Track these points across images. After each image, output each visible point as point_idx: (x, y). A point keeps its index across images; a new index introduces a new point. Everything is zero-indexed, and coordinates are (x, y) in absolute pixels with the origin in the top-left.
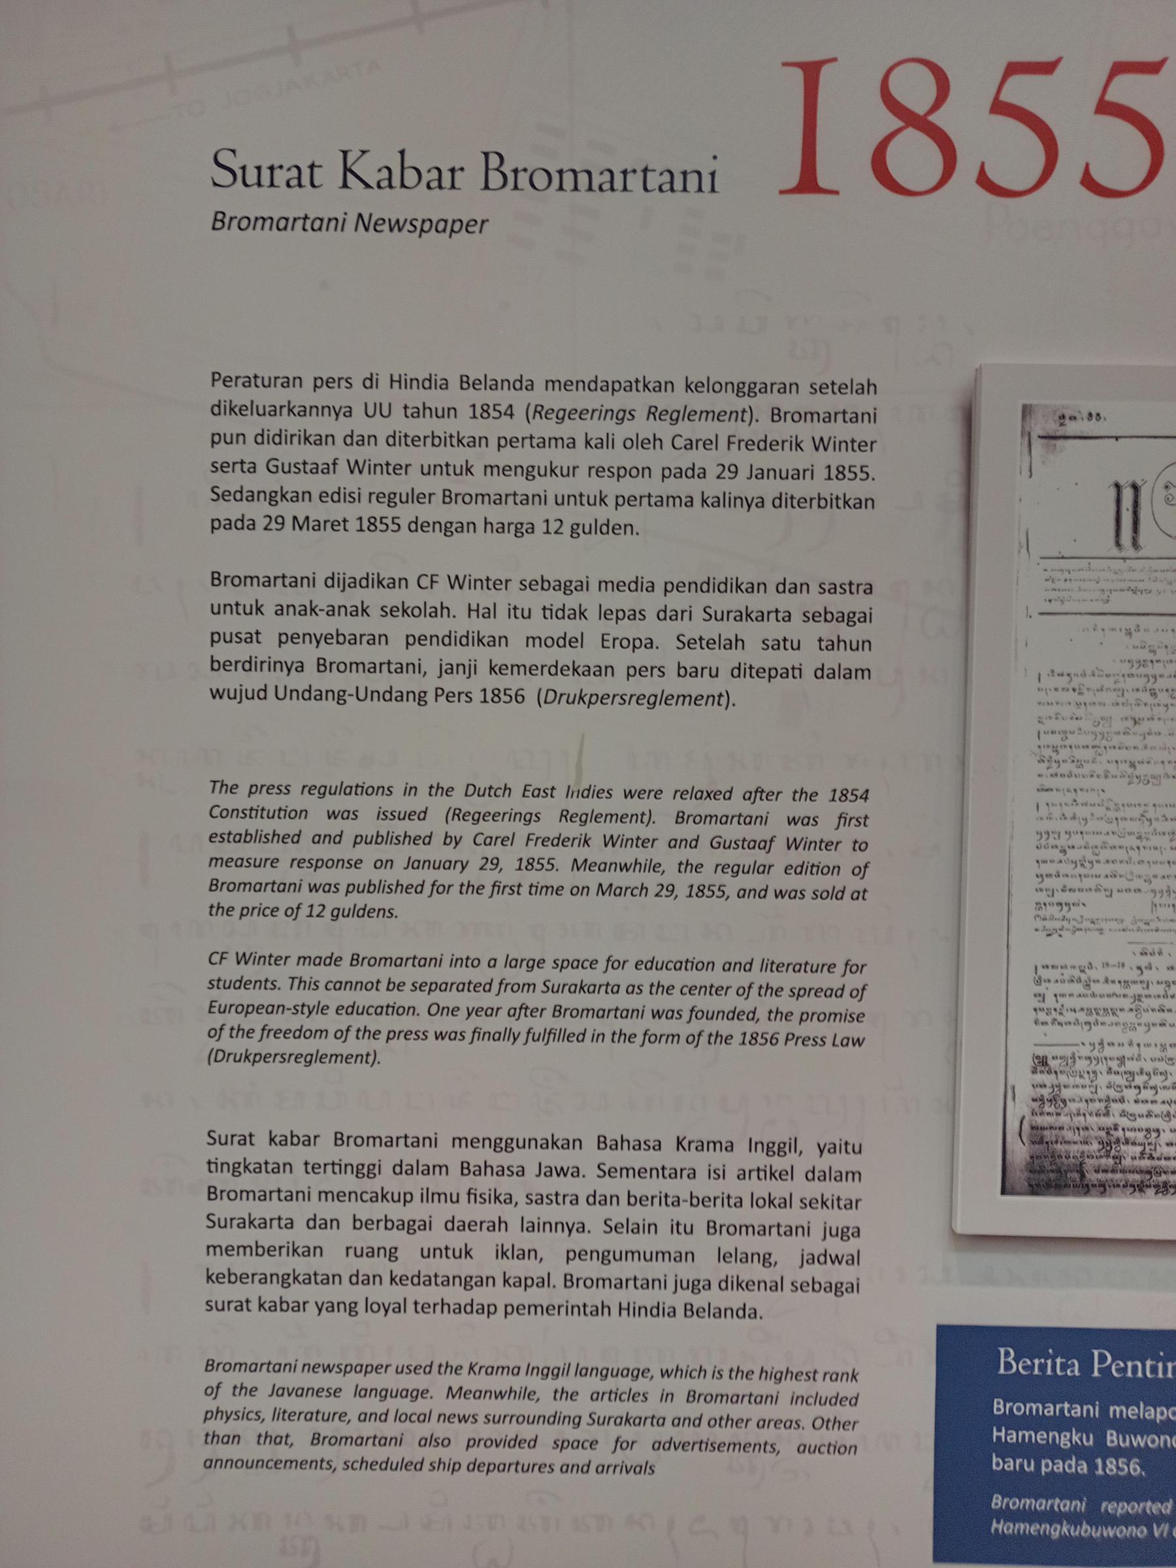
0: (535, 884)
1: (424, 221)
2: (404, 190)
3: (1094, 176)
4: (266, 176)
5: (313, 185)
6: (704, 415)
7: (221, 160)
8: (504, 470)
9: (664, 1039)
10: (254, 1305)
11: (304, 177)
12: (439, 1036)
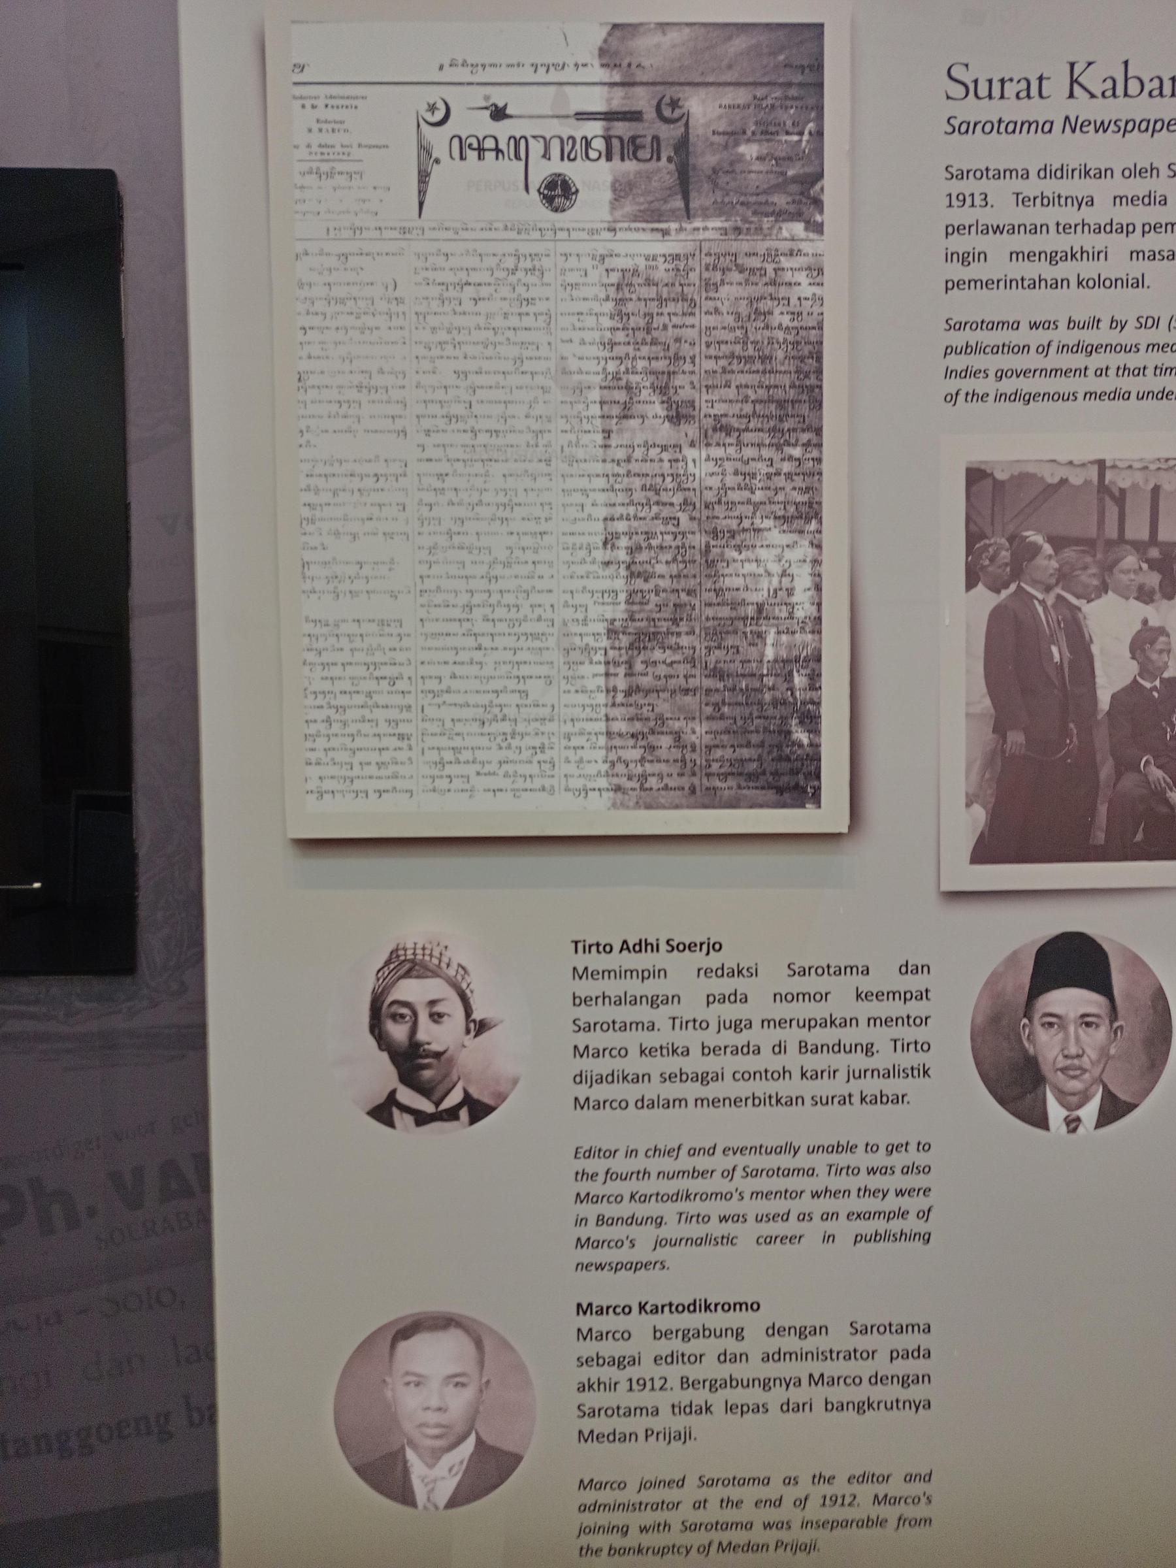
10: (856, 1099)
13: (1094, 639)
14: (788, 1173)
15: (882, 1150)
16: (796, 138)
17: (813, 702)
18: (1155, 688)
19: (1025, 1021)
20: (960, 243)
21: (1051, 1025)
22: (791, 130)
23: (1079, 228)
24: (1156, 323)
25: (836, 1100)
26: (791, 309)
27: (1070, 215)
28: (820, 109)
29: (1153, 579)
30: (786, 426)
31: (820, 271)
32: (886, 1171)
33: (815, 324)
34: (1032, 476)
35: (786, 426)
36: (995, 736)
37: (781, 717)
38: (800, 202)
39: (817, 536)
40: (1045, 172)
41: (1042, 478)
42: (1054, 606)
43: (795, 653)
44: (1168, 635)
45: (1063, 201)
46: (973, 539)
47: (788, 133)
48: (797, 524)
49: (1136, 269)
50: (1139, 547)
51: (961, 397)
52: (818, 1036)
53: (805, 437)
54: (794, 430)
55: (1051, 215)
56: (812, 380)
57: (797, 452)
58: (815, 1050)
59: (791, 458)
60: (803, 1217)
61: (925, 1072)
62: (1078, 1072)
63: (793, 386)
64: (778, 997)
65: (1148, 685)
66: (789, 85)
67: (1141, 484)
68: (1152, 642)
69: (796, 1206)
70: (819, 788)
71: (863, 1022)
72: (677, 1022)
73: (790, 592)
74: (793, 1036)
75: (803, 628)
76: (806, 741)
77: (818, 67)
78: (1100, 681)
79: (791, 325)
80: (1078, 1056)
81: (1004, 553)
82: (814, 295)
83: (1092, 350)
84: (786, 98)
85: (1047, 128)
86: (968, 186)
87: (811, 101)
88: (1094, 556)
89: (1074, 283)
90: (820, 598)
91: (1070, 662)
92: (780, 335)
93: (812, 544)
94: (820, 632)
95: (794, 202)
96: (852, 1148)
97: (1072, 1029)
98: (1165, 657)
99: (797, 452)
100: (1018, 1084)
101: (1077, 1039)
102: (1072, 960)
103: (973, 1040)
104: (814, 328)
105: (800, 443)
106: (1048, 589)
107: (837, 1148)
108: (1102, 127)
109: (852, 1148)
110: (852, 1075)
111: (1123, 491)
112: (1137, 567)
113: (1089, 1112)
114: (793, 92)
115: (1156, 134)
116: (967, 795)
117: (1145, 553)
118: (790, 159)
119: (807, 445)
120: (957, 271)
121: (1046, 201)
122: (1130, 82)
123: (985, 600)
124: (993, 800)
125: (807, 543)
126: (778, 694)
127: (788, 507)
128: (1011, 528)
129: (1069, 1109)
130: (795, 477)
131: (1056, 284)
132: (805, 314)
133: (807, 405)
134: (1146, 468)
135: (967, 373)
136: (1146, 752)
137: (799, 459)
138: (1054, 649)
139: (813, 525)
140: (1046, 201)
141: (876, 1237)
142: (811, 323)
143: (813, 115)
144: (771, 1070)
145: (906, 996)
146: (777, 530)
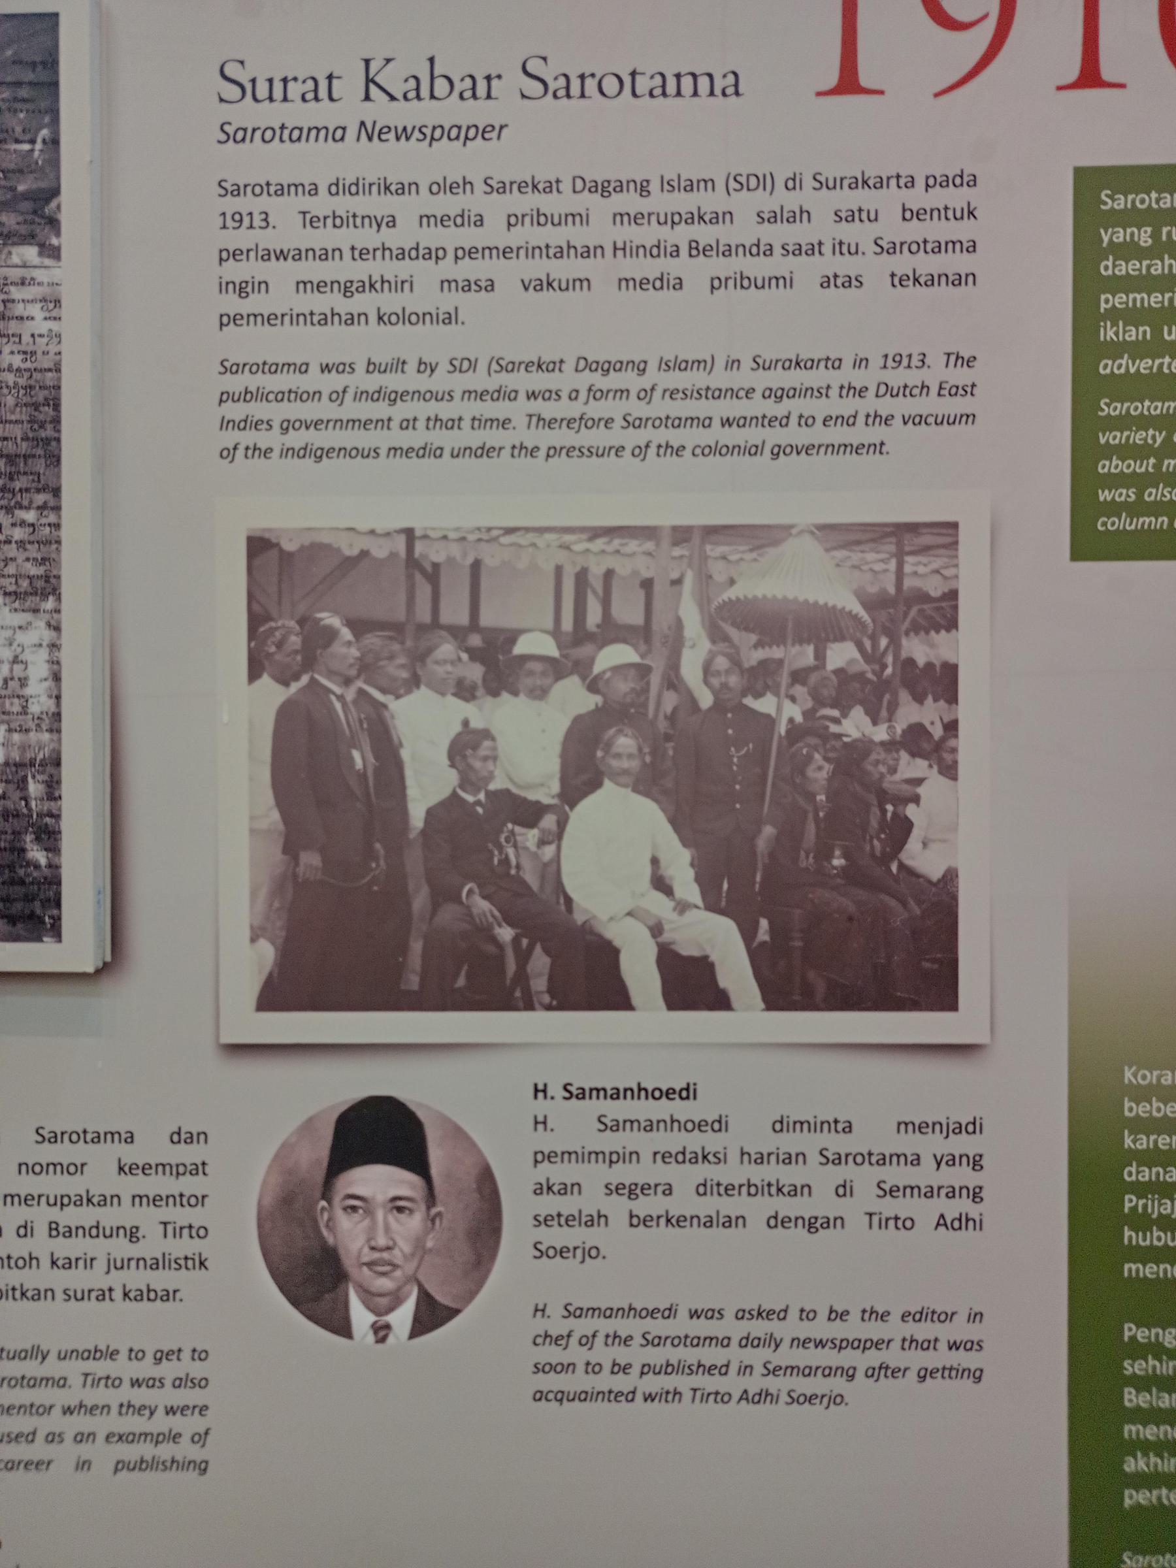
0: (478, 416)
1: (434, 128)
2: (434, 102)
5: (331, 99)
7: (529, 68)
8: (319, 287)
9: (611, 395)
10: (118, 1294)
11: (322, 88)
13: (404, 741)
14: (33, 1383)
15: (149, 1357)
16: (26, 147)
17: (51, 815)
18: (478, 803)
19: (323, 1203)
20: (236, 271)
21: (354, 1209)
22: (21, 138)
23: (379, 253)
24: (473, 365)
26: (23, 348)
27: (367, 237)
28: (55, 113)
29: (475, 672)
30: (17, 485)
31: (57, 302)
32: (155, 1383)
33: (51, 365)
34: (328, 547)
35: (17, 485)
36: (286, 857)
37: (13, 833)
38: (32, 223)
39: (55, 615)
40: (336, 187)
41: (338, 550)
42: (355, 702)
43: (29, 755)
44: (493, 739)
45: (359, 221)
46: (256, 621)
47: (17, 141)
48: (31, 601)
49: (448, 301)
50: (457, 633)
51: (240, 452)
52: (71, 1216)
53: (40, 499)
54: (27, 490)
55: (345, 238)
56: (49, 432)
57: (30, 516)
58: (69, 1233)
59: (23, 523)
60: (53, 1438)
61: (202, 1263)
62: (387, 1268)
63: (25, 438)
64: (24, 1168)
65: (470, 799)
66: (18, 84)
67: (458, 558)
68: (475, 747)
69: (45, 1425)
70: (60, 919)
71: (126, 1200)
72: (170, 1228)
73: (23, 682)
74: (41, 1216)
75: (38, 725)
76: (43, 861)
77: (51, 63)
78: (412, 791)
79: (23, 366)
80: (388, 1248)
81: (293, 638)
82: (50, 330)
83: (395, 397)
84: (16, 99)
85: (337, 135)
86: (244, 204)
87: (43, 105)
88: (403, 643)
89: (373, 318)
90: (59, 688)
91: (377, 771)
92: (10, 378)
93: (49, 625)
94: (59, 731)
95: (25, 221)
96: (113, 1354)
97: (380, 1215)
98: (490, 765)
99: (30, 516)
100: (315, 1281)
101: (387, 1229)
102: (380, 1132)
103: (260, 1226)
104: (50, 370)
105: (34, 505)
106: (347, 682)
107: (94, 1354)
108: (404, 134)
109: (113, 1354)
110: (114, 1265)
111: (436, 566)
112: (454, 657)
113: (402, 1317)
114: (24, 93)
115: (468, 142)
116: (252, 927)
117: (464, 640)
118: (21, 171)
119: (43, 508)
120: (232, 304)
121: (338, 221)
123: (271, 694)
124: (284, 933)
125: (42, 624)
126: (9, 805)
127: (20, 581)
128: (302, 608)
129: (378, 1313)
130: (28, 546)
131: (351, 320)
132: (39, 353)
133: (43, 460)
134: (463, 539)
135: (246, 424)
136: (469, 878)
137: (33, 525)
138: (356, 755)
139: (50, 604)
140: (338, 221)
141: (142, 1465)
142: (47, 363)
143: (47, 119)
144: (15, 1255)
145: (178, 1170)
146: (7, 609)
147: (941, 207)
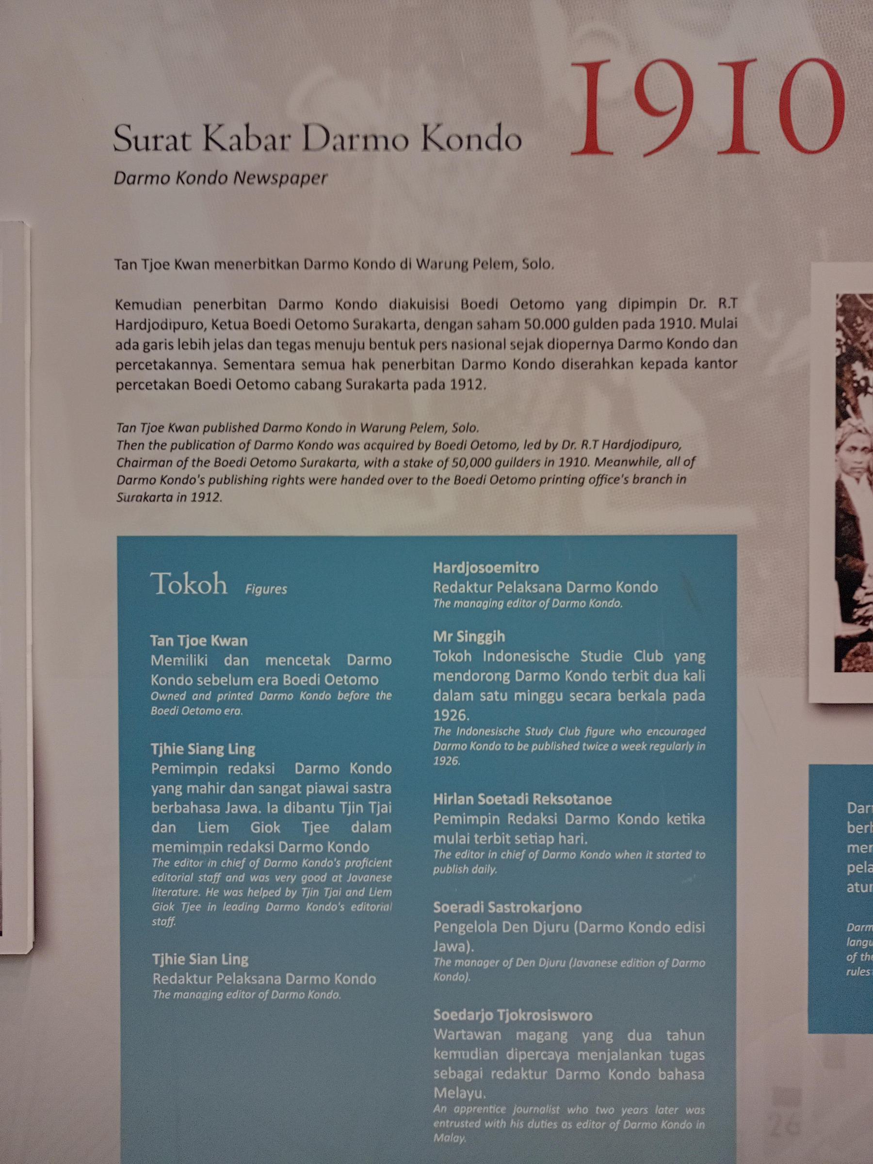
1: (282, 177)
2: (249, 152)
3: (730, 146)
4: (152, 143)
5: (184, 148)
6: (149, 179)
7: (119, 132)
12: (313, 481)
25: (366, 385)
122: (251, 139)
147: (717, 360)
